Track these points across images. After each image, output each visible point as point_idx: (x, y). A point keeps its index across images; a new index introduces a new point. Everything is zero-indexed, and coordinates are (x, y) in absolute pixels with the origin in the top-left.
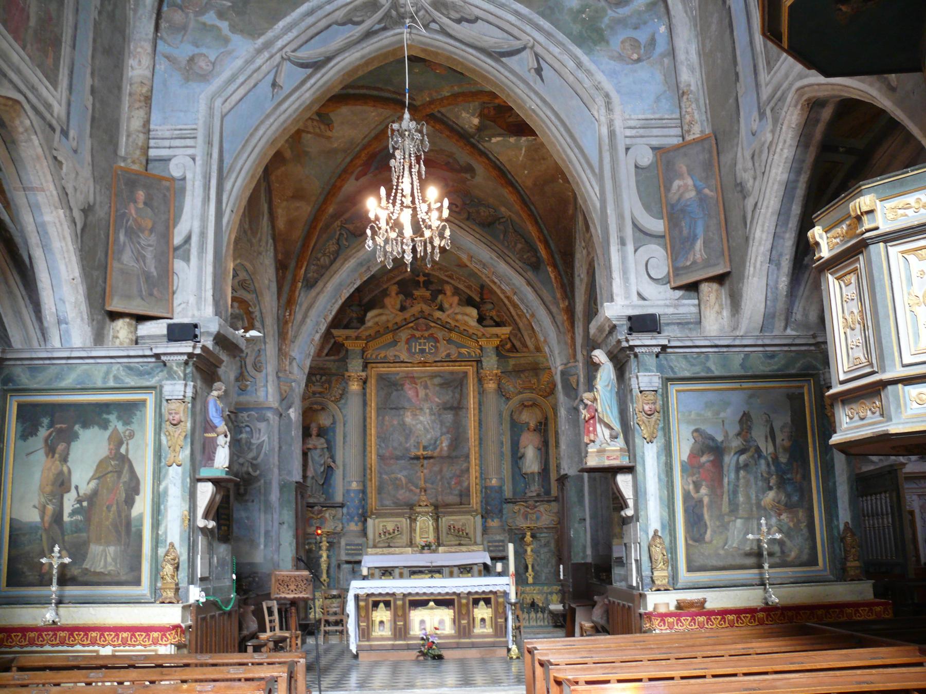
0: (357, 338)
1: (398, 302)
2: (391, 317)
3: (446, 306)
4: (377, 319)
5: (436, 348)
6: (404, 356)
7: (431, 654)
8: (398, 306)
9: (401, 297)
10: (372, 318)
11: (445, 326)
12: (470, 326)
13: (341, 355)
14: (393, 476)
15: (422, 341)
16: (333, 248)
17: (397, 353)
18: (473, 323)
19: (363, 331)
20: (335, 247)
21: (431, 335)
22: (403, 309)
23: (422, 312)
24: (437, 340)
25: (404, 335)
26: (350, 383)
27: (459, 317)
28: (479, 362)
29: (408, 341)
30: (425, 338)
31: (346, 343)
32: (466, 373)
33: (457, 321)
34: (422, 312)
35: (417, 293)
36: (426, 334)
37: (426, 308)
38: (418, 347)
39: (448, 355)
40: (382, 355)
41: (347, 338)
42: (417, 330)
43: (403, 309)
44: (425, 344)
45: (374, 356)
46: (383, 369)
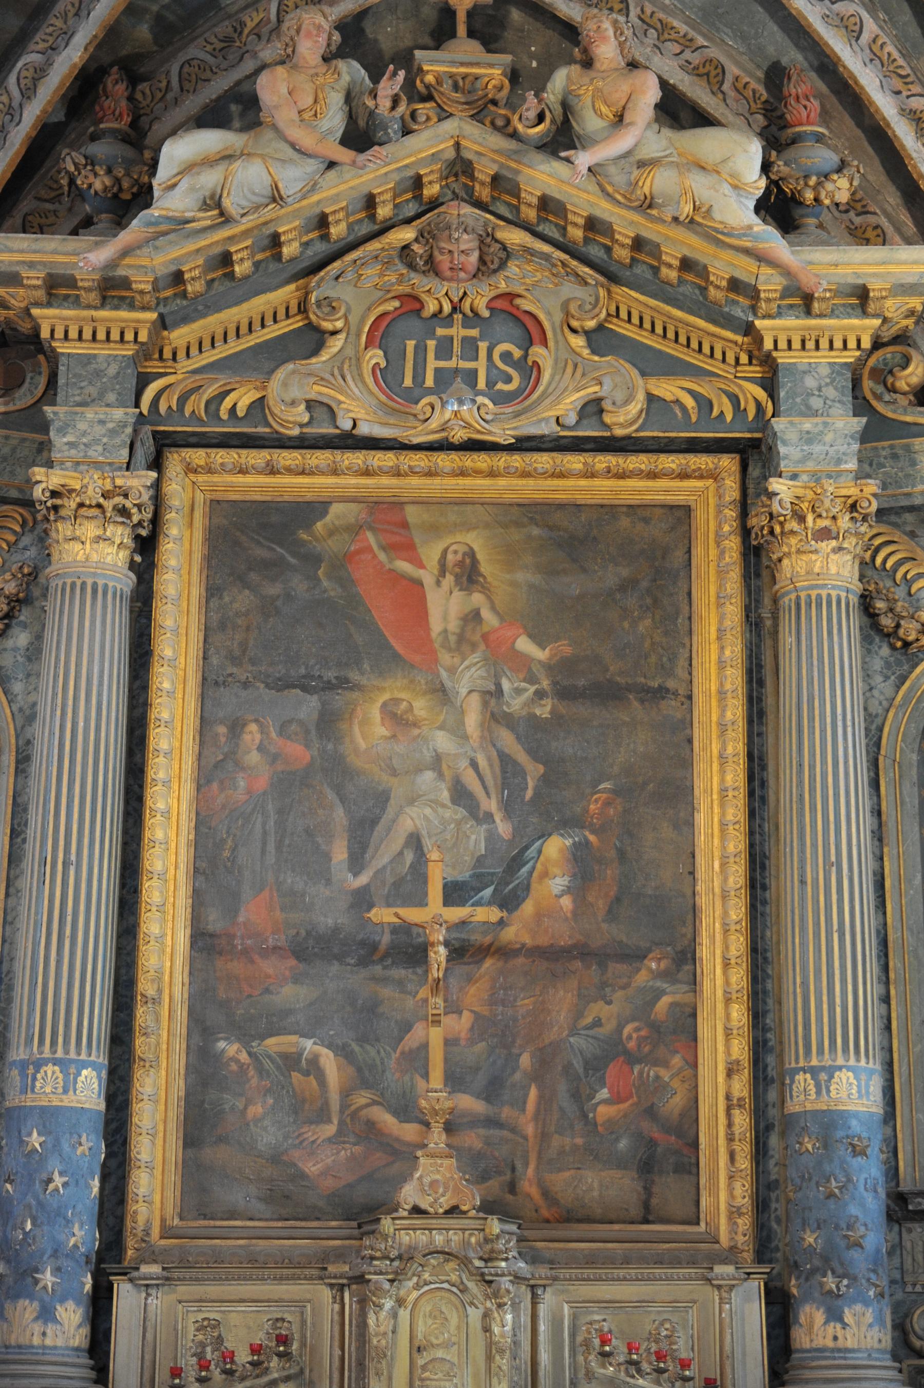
0: (113, 290)
1: (336, 99)
2: (293, 177)
3: (590, 122)
4: (209, 179)
5: (530, 371)
6: (359, 410)
7: (293, 51)
8: (334, 120)
9: (351, 71)
10: (189, 168)
11: (591, 251)
12: (717, 237)
13: (23, 398)
14: (273, 1044)
15: (458, 331)
16: (93, 391)
17: (317, 391)
18: (739, 212)
19: (142, 251)
20: (95, 394)
21: (507, 307)
22: (360, 136)
23: (460, 167)
24: (530, 331)
25: (356, 293)
26: (63, 529)
27: (661, 182)
28: (754, 453)
29: (382, 333)
30: (473, 319)
31: (50, 319)
32: (681, 515)
33: (647, 205)
34: (460, 167)
35: (434, 65)
36: (480, 298)
37: (484, 146)
38: (432, 364)
39: (594, 408)
40: (243, 398)
41: (58, 287)
42: (432, 267)
43: (360, 136)
44: (470, 347)
45: (197, 404)
46: (248, 477)
